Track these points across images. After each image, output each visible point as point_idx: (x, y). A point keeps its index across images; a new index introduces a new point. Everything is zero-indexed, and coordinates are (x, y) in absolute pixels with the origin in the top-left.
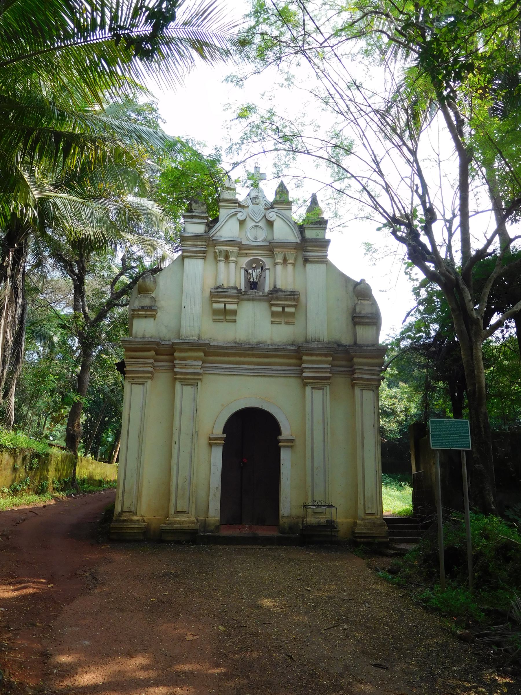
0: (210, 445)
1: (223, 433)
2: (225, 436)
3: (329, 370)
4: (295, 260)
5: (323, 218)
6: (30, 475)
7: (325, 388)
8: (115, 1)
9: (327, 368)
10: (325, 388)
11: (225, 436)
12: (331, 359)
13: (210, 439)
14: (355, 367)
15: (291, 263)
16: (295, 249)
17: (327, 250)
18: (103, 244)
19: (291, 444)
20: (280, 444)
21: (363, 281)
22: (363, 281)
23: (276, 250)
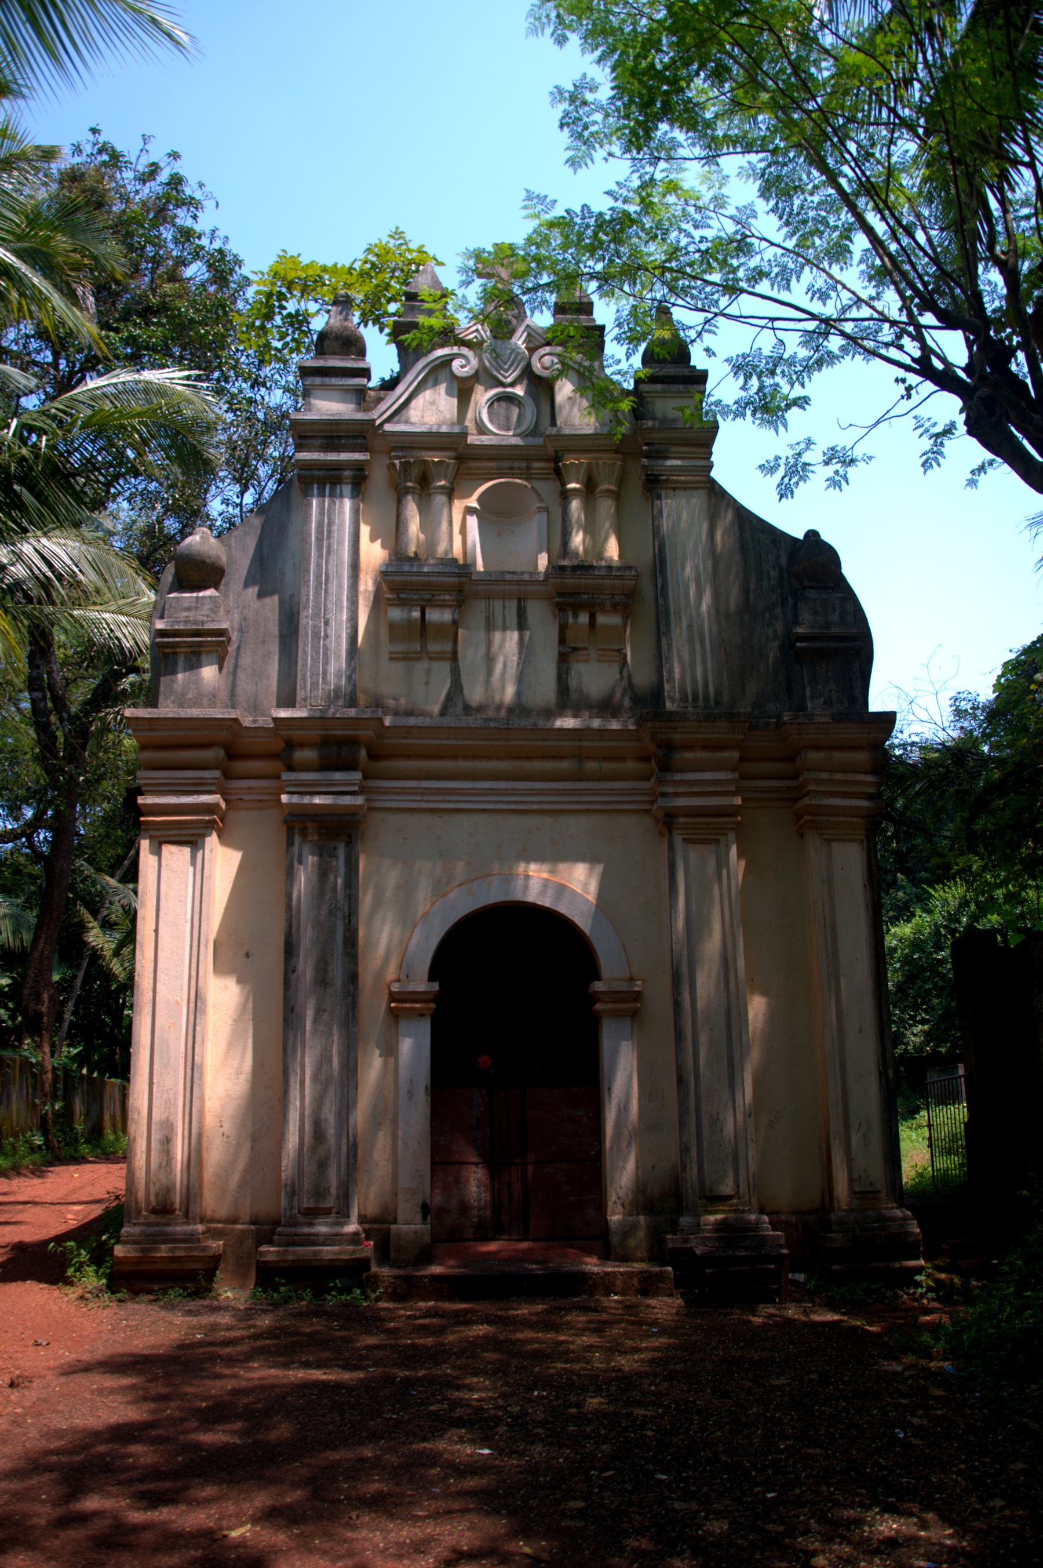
0: (395, 1016)
1: (432, 978)
2: (436, 986)
3: (733, 788)
4: (621, 481)
5: (694, 367)
6: (963, 1374)
7: (722, 839)
8: (4, 1485)
9: (726, 782)
10: (722, 839)
11: (436, 986)
12: (736, 755)
13: (393, 997)
14: (806, 775)
15: (608, 491)
16: (616, 452)
17: (711, 454)
18: (72, 415)
19: (632, 1005)
20: (598, 1006)
21: (812, 536)
22: (812, 536)
23: (570, 460)
